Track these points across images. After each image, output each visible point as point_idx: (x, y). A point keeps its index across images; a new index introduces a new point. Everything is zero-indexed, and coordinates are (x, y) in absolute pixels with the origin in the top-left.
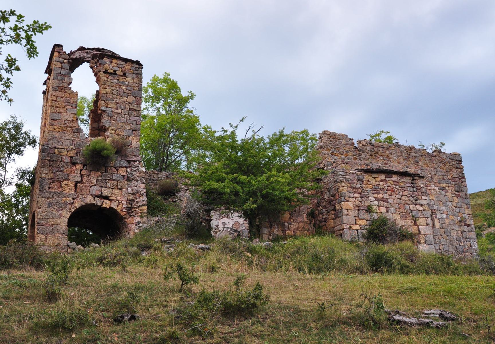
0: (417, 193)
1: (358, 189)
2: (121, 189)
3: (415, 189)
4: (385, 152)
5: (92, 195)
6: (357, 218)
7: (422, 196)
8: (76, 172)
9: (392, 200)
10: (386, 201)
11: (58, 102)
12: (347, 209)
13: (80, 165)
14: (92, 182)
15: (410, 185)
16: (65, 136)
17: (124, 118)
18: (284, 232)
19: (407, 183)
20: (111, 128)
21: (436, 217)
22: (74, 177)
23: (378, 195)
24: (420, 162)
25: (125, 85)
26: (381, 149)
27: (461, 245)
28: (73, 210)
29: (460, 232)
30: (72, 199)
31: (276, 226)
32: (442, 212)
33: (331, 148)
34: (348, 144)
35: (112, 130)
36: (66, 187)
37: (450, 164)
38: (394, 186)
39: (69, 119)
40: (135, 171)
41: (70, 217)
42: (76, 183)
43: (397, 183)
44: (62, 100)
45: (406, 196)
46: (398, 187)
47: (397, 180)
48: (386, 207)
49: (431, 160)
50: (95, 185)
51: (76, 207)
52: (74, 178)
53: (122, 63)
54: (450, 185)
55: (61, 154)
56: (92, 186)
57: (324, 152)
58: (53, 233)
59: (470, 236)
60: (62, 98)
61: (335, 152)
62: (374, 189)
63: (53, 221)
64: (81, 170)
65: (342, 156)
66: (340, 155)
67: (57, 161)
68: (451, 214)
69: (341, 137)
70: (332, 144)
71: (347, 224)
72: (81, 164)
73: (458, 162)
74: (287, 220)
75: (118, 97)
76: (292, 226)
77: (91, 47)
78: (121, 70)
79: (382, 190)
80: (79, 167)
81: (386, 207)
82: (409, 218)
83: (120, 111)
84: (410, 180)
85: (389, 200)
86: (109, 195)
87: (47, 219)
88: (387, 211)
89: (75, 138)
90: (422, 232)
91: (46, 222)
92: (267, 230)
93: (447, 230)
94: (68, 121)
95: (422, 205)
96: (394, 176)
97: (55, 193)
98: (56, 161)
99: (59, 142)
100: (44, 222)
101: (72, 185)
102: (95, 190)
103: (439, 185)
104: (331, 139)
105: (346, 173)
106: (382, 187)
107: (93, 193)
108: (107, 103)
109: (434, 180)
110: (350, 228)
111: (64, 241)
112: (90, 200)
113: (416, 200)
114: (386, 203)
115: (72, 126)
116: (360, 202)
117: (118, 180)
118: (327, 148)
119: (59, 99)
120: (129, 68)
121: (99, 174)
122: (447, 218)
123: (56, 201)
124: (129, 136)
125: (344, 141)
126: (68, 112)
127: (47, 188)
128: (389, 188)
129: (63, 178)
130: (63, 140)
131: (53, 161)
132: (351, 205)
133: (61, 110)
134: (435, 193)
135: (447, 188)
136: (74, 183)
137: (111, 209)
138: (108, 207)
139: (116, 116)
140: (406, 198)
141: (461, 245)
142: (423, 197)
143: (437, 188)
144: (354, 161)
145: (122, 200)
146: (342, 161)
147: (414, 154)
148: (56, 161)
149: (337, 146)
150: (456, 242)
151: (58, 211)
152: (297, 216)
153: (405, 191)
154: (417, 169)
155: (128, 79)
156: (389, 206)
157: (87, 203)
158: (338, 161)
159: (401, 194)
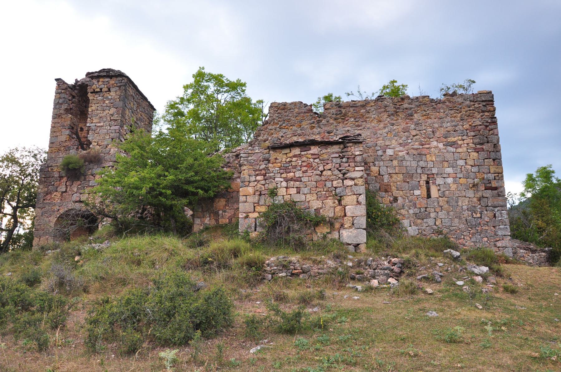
0: (347, 165)
1: (261, 170)
3: (344, 160)
4: (359, 112)
5: (73, 202)
6: (255, 205)
7: (356, 166)
9: (307, 178)
10: (299, 180)
12: (246, 196)
13: (65, 178)
15: (337, 155)
17: (105, 129)
18: (217, 221)
19: (333, 153)
21: (434, 183)
23: (288, 174)
24: (415, 115)
25: (108, 99)
26: (351, 109)
27: (475, 216)
29: (475, 200)
31: (208, 215)
32: (445, 176)
33: (279, 121)
34: (302, 113)
35: (95, 142)
36: (56, 197)
37: (471, 108)
38: (312, 160)
42: (63, 192)
43: (316, 156)
44: (59, 125)
45: (330, 170)
46: (317, 160)
47: (316, 153)
48: (297, 188)
49: (435, 108)
54: (465, 137)
57: (270, 127)
59: (495, 203)
61: (284, 125)
62: (283, 168)
64: (67, 182)
65: (294, 128)
66: (291, 127)
68: (462, 176)
69: (292, 106)
70: (280, 116)
71: (244, 213)
73: (484, 104)
74: (222, 207)
76: (226, 214)
77: (97, 71)
78: (106, 87)
79: (295, 167)
80: (65, 179)
81: (297, 188)
82: (330, 198)
83: (102, 124)
84: (339, 148)
88: (298, 192)
90: (349, 214)
92: (200, 220)
93: (453, 199)
95: (353, 179)
96: (312, 147)
97: (46, 203)
101: (59, 194)
102: (75, 197)
103: (445, 140)
104: (279, 111)
105: (249, 154)
106: (293, 164)
107: (74, 200)
109: (437, 134)
110: (247, 217)
112: (71, 206)
113: (344, 174)
114: (298, 183)
116: (264, 185)
118: (274, 122)
120: (113, 82)
121: (79, 182)
122: (455, 182)
124: (108, 145)
125: (297, 110)
126: (63, 134)
127: (42, 200)
128: (304, 164)
132: (250, 190)
133: (58, 134)
134: (437, 152)
135: (460, 142)
139: (98, 129)
140: (329, 173)
141: (475, 216)
142: (357, 169)
143: (441, 145)
144: (310, 131)
146: (293, 134)
147: (406, 106)
149: (287, 118)
150: (466, 213)
152: (234, 203)
153: (327, 164)
154: (409, 125)
155: (111, 93)
156: (301, 186)
158: (288, 134)
159: (321, 168)
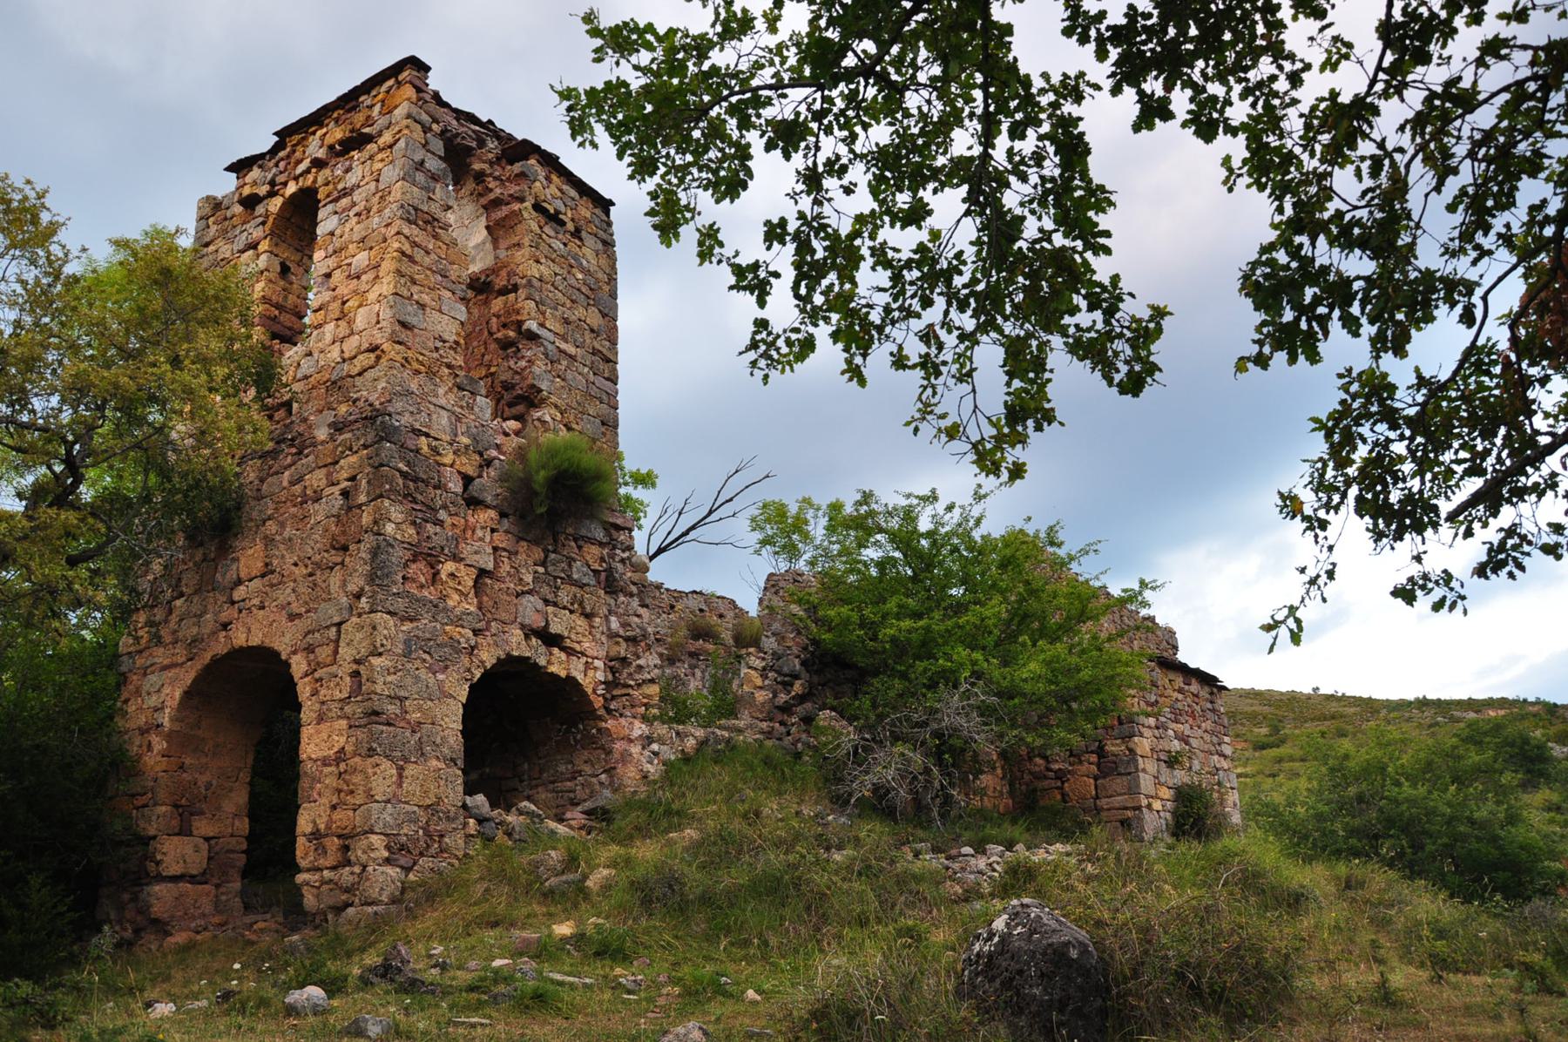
2: (589, 616)
5: (523, 627)
8: (479, 533)
11: (415, 262)
13: (492, 513)
14: (521, 579)
16: (436, 396)
20: (553, 399)
22: (476, 553)
28: (478, 674)
30: (470, 634)
39: (447, 338)
40: (623, 561)
41: (468, 699)
50: (530, 592)
51: (482, 662)
52: (477, 557)
53: (573, 193)
55: (438, 458)
56: (523, 593)
58: (422, 754)
60: (428, 253)
63: (420, 709)
67: (426, 483)
72: (494, 508)
75: (568, 303)
85: (1191, 740)
86: (566, 634)
87: (402, 699)
89: (462, 407)
91: (398, 711)
94: (444, 342)
98: (423, 481)
99: (420, 411)
100: (392, 709)
102: (530, 611)
107: (527, 621)
108: (543, 313)
111: (453, 791)
112: (517, 643)
115: (454, 362)
117: (585, 585)
119: (419, 255)
120: (588, 215)
123: (428, 636)
129: (446, 551)
130: (432, 407)
131: (416, 480)
133: (426, 298)
136: (474, 573)
137: (571, 680)
138: (563, 674)
145: (595, 654)
148: (423, 481)
151: (434, 674)
157: (508, 655)
